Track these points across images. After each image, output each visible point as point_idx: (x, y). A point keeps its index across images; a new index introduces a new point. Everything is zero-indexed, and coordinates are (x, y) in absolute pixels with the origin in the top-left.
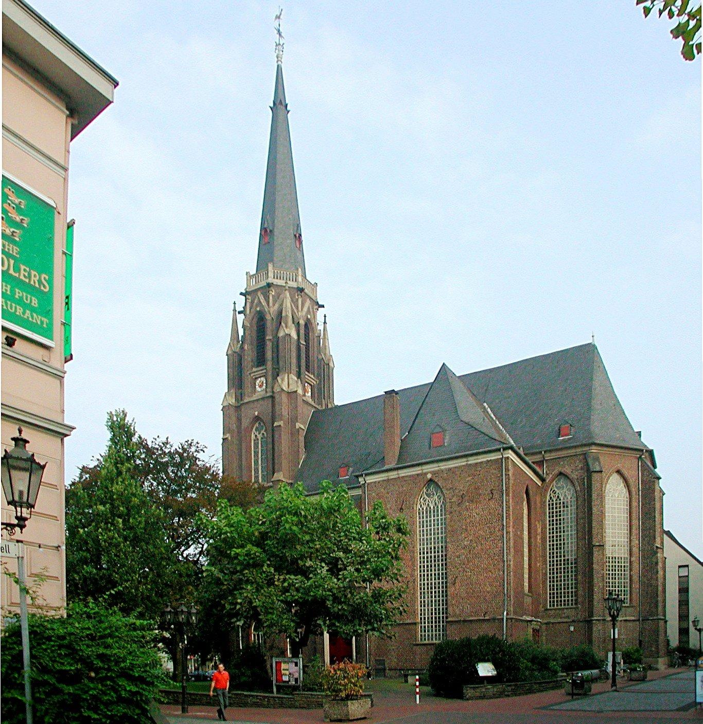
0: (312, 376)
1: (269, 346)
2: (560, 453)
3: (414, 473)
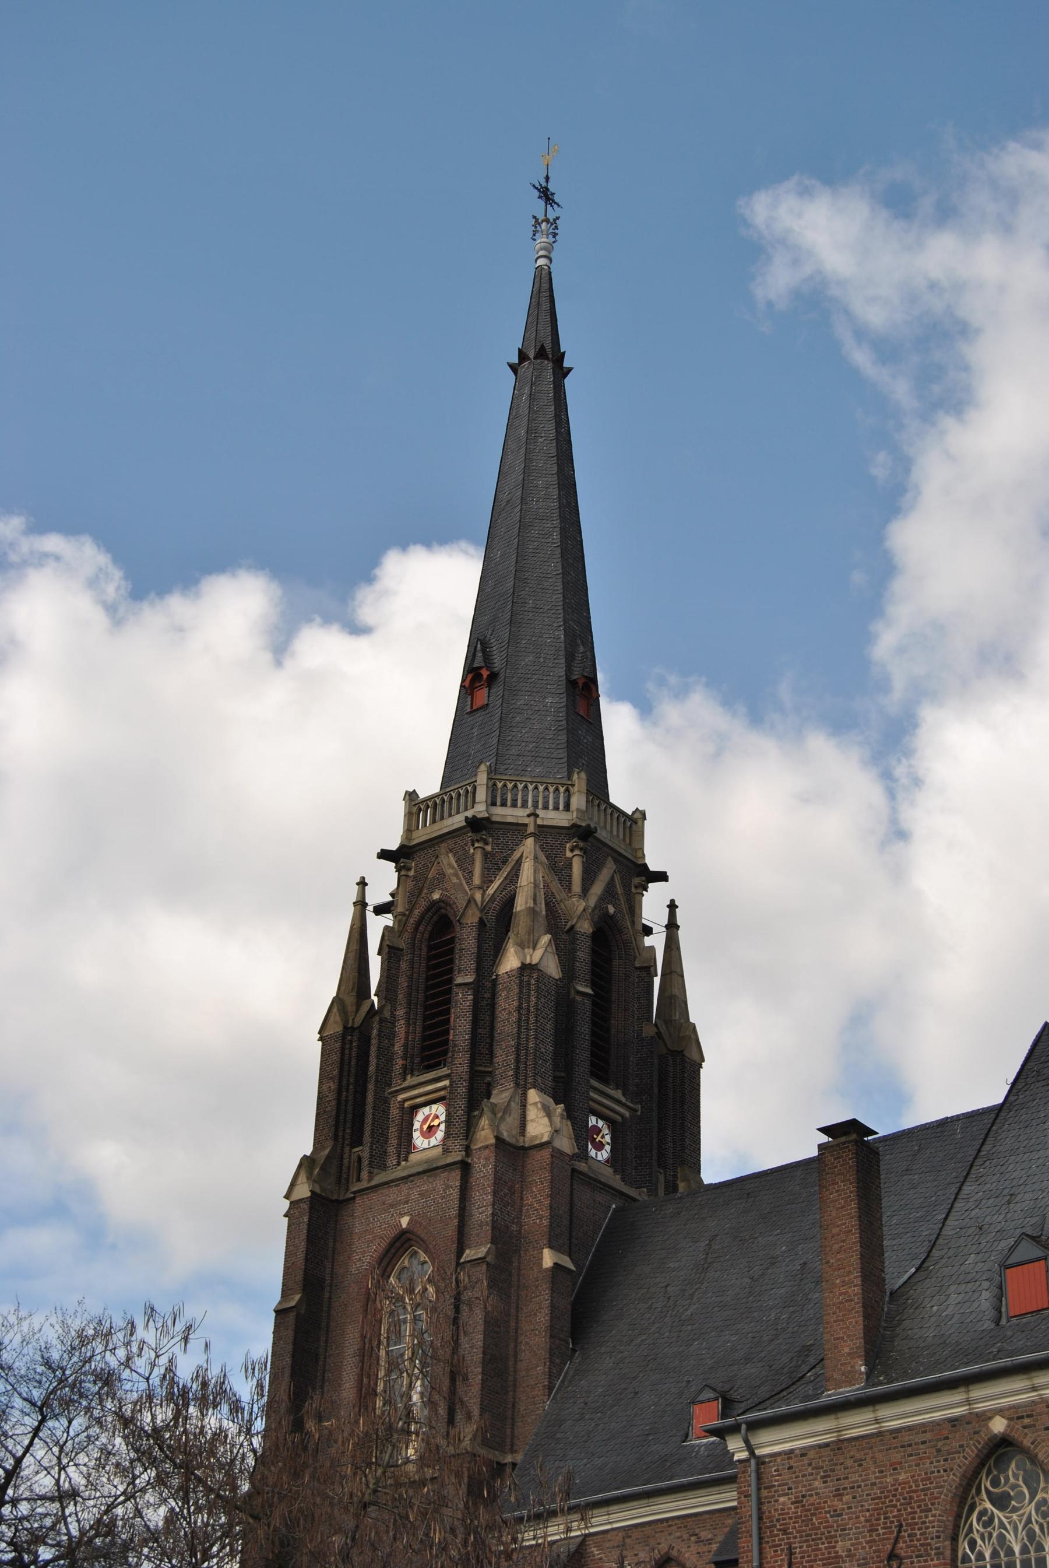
0: (618, 1094)
1: (463, 1003)
2: (599, 1098)
3: (937, 1415)
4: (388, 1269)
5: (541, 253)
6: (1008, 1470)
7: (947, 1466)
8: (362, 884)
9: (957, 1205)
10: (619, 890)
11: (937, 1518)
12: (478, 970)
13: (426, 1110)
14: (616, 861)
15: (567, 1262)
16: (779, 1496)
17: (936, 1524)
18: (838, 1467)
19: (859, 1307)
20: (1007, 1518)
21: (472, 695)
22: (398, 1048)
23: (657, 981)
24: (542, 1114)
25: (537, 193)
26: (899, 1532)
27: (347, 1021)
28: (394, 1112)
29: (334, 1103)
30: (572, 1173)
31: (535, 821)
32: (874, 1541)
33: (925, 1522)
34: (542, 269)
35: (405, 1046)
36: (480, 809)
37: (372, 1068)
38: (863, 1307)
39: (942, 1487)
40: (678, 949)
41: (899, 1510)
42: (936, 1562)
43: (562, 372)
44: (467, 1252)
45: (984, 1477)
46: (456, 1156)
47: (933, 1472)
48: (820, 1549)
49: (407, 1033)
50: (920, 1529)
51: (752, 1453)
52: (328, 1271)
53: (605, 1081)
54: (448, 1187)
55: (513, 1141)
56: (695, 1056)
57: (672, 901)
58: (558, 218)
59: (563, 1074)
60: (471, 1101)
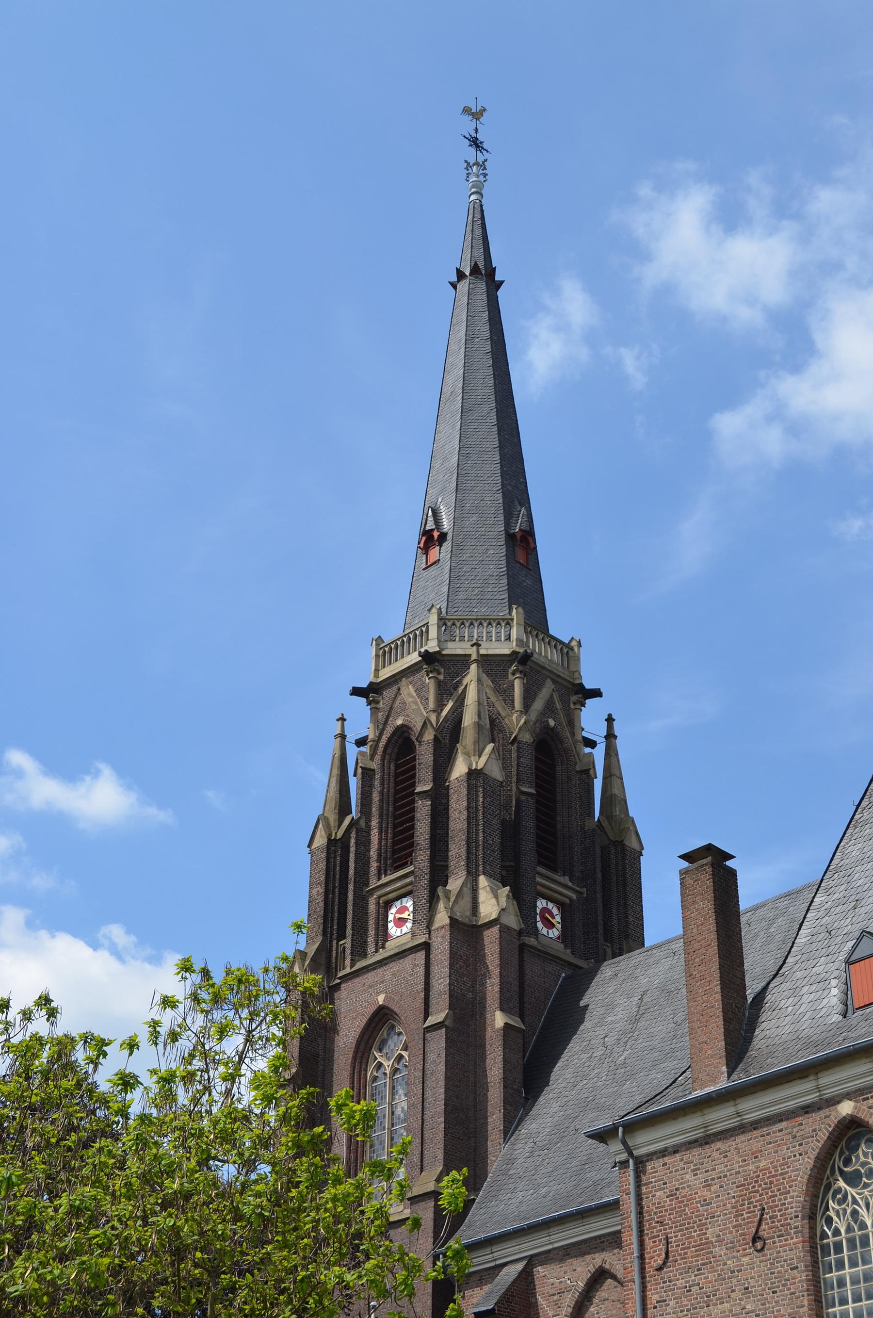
0: (566, 880)
1: (423, 809)
2: (547, 883)
4: (371, 1042)
5: (473, 190)
6: (858, 1149)
7: (802, 1149)
9: (809, 915)
10: (558, 706)
11: (795, 1198)
12: (435, 780)
13: (398, 904)
14: (554, 681)
15: (516, 1022)
16: (656, 1191)
17: (794, 1205)
18: (706, 1160)
19: (719, 1012)
20: (858, 1194)
21: (426, 553)
22: (373, 853)
24: (491, 895)
25: (468, 142)
26: (762, 1215)
27: (330, 835)
28: (372, 907)
29: (322, 904)
30: (520, 946)
31: (478, 651)
32: (741, 1225)
33: (784, 1204)
34: (475, 203)
35: (379, 850)
36: (432, 646)
37: (351, 872)
38: (723, 1012)
39: (798, 1170)
40: (617, 755)
41: (761, 1195)
42: (795, 1240)
43: (494, 286)
44: (430, 1018)
45: (837, 1158)
46: (421, 939)
47: (790, 1157)
48: (693, 1237)
49: (380, 840)
50: (779, 1211)
51: (631, 1154)
52: (321, 1047)
53: (555, 870)
54: (415, 966)
55: (467, 921)
56: (635, 845)
57: (610, 715)
58: (486, 160)
59: (512, 864)
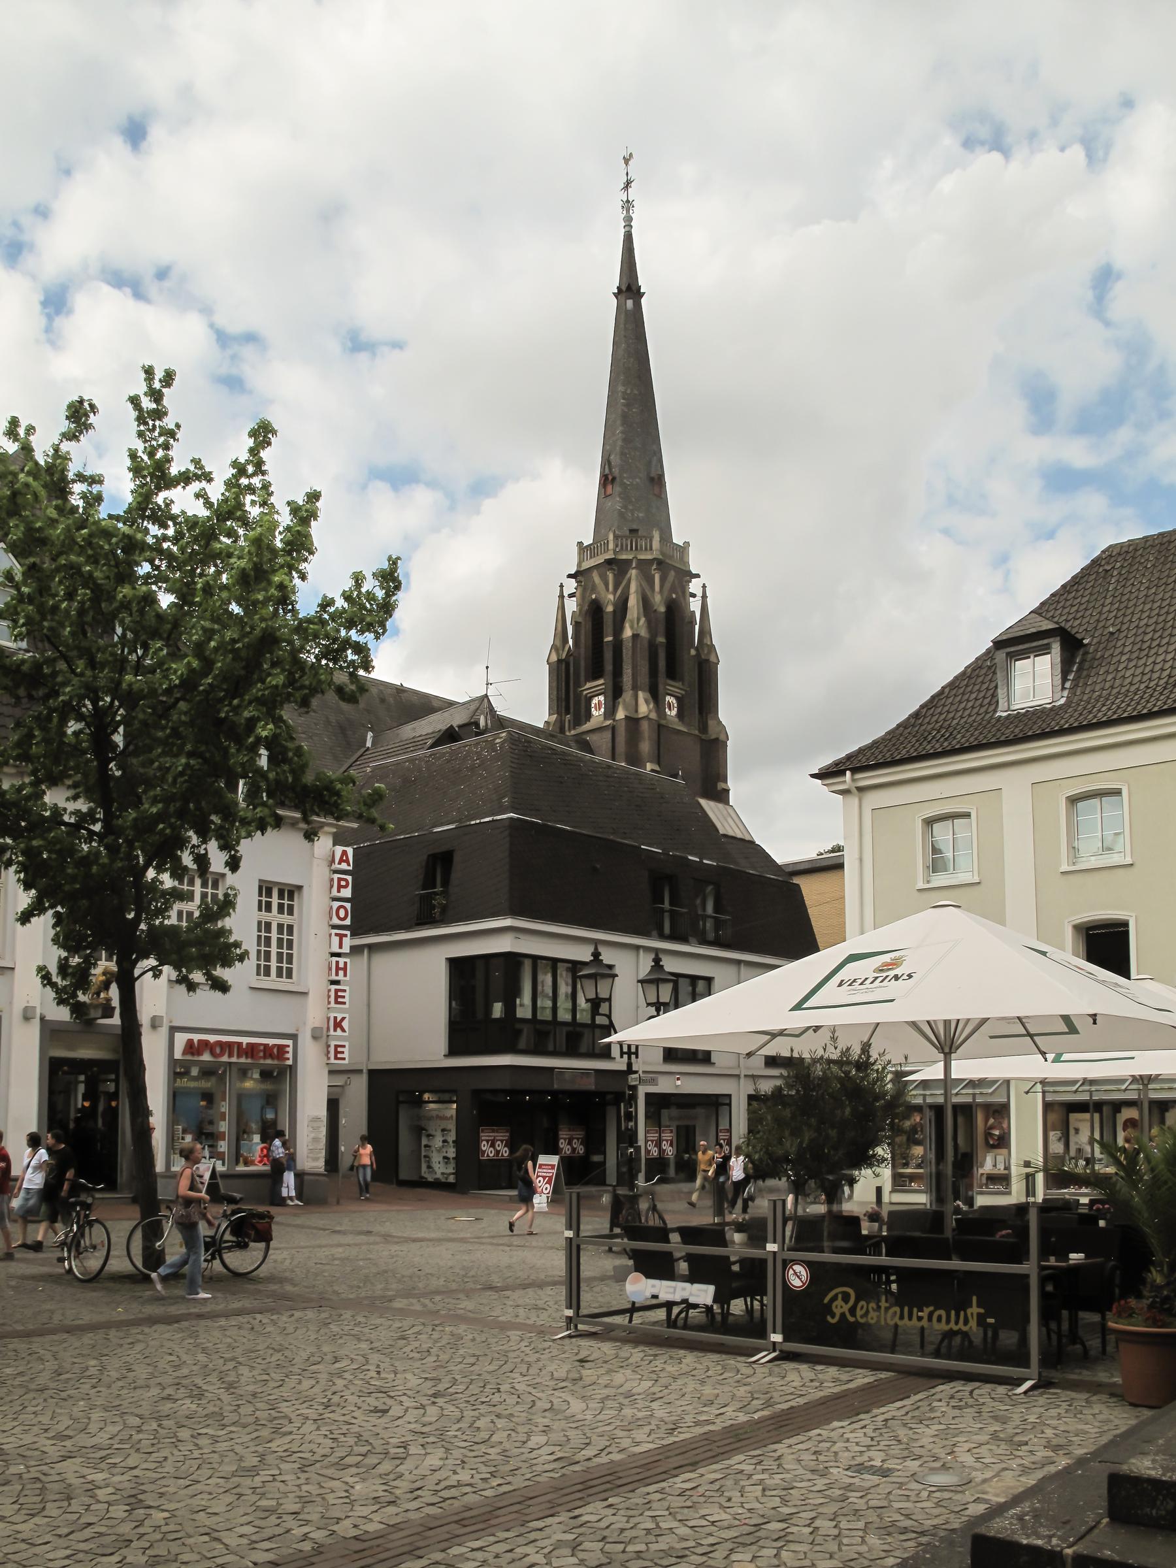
8: (561, 586)
23: (697, 627)
60: (615, 693)
